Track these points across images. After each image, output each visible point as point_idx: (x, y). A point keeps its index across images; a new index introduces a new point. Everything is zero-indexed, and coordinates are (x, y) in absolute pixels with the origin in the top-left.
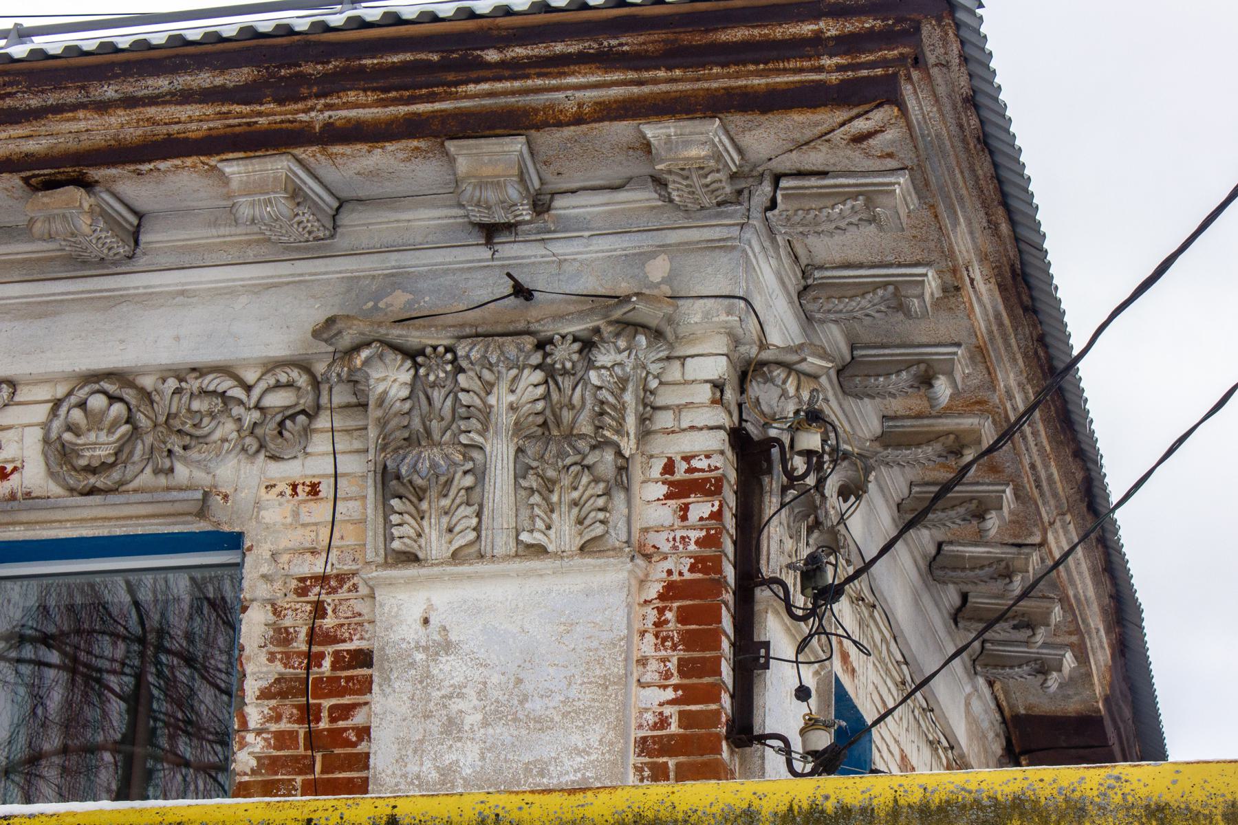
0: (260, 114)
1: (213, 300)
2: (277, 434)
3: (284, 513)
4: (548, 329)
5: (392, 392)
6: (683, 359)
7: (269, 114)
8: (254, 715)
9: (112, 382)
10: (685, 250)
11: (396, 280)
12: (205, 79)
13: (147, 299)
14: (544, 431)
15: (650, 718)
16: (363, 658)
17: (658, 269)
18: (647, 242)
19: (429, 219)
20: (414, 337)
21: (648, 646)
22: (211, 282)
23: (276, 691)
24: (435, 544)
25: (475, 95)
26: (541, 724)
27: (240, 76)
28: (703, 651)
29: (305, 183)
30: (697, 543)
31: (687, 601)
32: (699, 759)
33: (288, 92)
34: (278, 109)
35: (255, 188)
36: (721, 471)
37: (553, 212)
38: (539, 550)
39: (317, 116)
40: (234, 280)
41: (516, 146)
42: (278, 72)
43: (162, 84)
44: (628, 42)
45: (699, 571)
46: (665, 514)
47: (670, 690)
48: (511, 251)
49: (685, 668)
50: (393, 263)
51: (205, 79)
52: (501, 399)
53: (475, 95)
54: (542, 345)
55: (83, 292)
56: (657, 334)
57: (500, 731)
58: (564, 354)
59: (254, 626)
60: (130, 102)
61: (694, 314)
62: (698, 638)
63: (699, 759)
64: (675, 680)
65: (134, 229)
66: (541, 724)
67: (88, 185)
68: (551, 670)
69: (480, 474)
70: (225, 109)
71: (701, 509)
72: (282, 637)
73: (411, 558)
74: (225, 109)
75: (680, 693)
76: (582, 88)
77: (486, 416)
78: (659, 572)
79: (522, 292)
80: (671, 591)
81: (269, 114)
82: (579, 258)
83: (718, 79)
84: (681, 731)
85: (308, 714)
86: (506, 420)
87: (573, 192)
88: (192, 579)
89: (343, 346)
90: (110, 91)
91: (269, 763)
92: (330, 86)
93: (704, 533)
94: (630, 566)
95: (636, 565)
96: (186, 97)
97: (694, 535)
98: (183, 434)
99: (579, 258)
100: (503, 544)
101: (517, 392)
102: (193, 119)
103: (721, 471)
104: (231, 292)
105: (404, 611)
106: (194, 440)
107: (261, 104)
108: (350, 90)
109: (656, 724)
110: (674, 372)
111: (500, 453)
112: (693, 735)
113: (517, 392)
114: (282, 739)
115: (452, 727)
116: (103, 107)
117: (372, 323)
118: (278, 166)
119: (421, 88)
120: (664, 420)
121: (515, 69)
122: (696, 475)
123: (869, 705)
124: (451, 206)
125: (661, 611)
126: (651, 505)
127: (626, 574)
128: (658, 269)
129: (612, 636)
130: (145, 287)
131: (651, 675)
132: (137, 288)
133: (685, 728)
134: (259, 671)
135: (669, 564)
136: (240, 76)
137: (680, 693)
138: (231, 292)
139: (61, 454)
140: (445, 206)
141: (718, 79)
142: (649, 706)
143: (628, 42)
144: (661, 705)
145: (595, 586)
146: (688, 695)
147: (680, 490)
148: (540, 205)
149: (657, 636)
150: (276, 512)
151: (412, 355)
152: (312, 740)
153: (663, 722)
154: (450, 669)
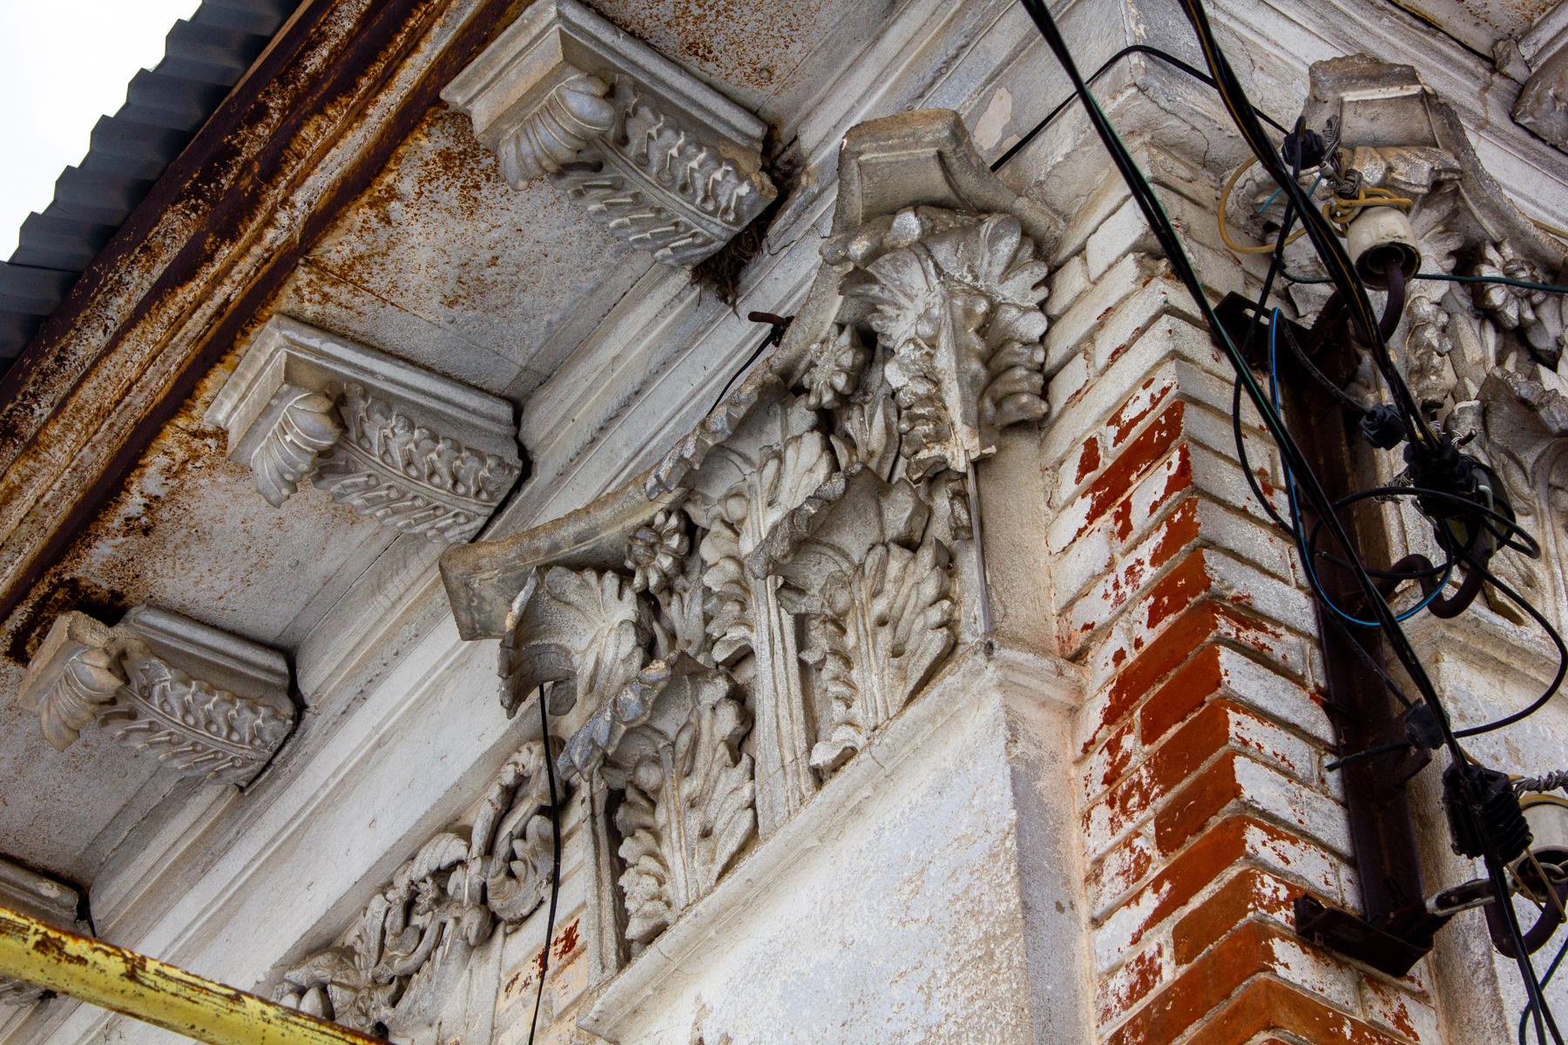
0: (217, 281)
5: (608, 657)
6: (1080, 251)
10: (1028, 55)
15: (1121, 983)
19: (646, 330)
22: (410, 694)
28: (1196, 767)
29: (372, 373)
30: (1153, 563)
32: (1223, 1008)
34: (236, 249)
36: (1173, 391)
37: (814, 163)
40: (435, 668)
42: (219, 188)
45: (1167, 612)
47: (1149, 893)
50: (626, 454)
55: (267, 846)
63: (1223, 1008)
64: (1158, 865)
68: (896, 993)
70: (173, 311)
74: (173, 311)
75: (1167, 886)
78: (1101, 672)
84: (1185, 967)
87: (1095, 232)
93: (1164, 530)
94: (991, 673)
95: (1010, 666)
97: (1146, 551)
103: (1173, 391)
107: (210, 259)
108: (299, 127)
109: (1132, 987)
112: (1200, 962)
117: (517, 538)
119: (391, 40)
122: (1135, 433)
123: (784, 289)
124: (664, 278)
125: (1113, 746)
127: (996, 699)
129: (989, 839)
130: (334, 775)
131: (1113, 887)
132: (326, 784)
133: (1188, 961)
135: (1118, 640)
137: (1167, 886)
140: (655, 286)
142: (1115, 959)
144: (1136, 940)
145: (949, 764)
149: (1111, 803)
153: (1147, 971)
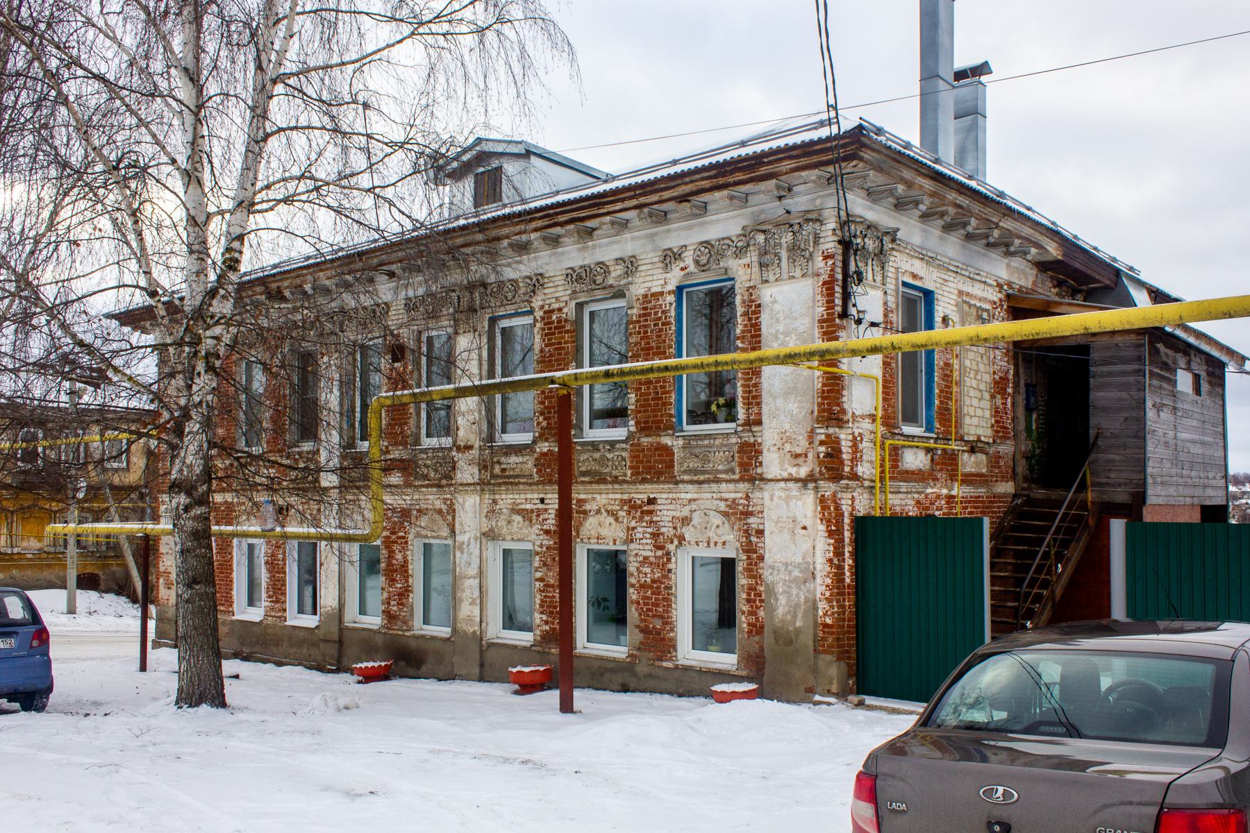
1: (724, 221)
2: (740, 252)
3: (742, 271)
4: (792, 222)
7: (721, 181)
8: (739, 320)
9: (706, 243)
11: (762, 212)
12: (706, 174)
13: (710, 223)
14: (794, 249)
16: (759, 305)
17: (818, 202)
18: (815, 195)
20: (763, 227)
21: (819, 297)
23: (745, 314)
24: (772, 278)
25: (764, 170)
26: (796, 319)
27: (713, 173)
31: (829, 285)
33: (723, 175)
35: (721, 198)
38: (793, 277)
39: (731, 179)
41: (774, 181)
43: (698, 176)
44: (794, 153)
46: (822, 264)
48: (784, 201)
49: (828, 302)
51: (706, 174)
52: (783, 240)
53: (764, 170)
54: (791, 226)
56: (818, 220)
57: (788, 321)
58: (796, 228)
59: (738, 300)
60: (692, 182)
61: (826, 213)
62: (830, 294)
65: (704, 207)
66: (796, 319)
67: (688, 201)
69: (780, 259)
71: (830, 262)
72: (744, 302)
73: (767, 281)
76: (786, 165)
77: (780, 244)
78: (821, 279)
79: (788, 212)
80: (825, 283)
81: (721, 181)
82: (800, 202)
83: (815, 159)
85: (750, 319)
86: (785, 245)
88: (157, 645)
89: (747, 234)
90: (687, 180)
91: (743, 331)
92: (732, 172)
96: (703, 179)
98: (721, 255)
99: (800, 202)
100: (785, 276)
101: (787, 238)
102: (706, 184)
104: (727, 219)
105: (767, 294)
106: (723, 256)
110: (824, 228)
111: (784, 254)
113: (787, 238)
114: (745, 326)
115: (778, 321)
116: (686, 184)
118: (725, 192)
120: (822, 240)
121: (770, 163)
126: (819, 262)
128: (818, 202)
134: (740, 310)
136: (713, 173)
138: (727, 219)
139: (697, 262)
141: (815, 159)
143: (794, 153)
146: (828, 308)
147: (826, 258)
148: (790, 190)
150: (741, 272)
151: (764, 232)
152: (752, 325)
154: (777, 307)
